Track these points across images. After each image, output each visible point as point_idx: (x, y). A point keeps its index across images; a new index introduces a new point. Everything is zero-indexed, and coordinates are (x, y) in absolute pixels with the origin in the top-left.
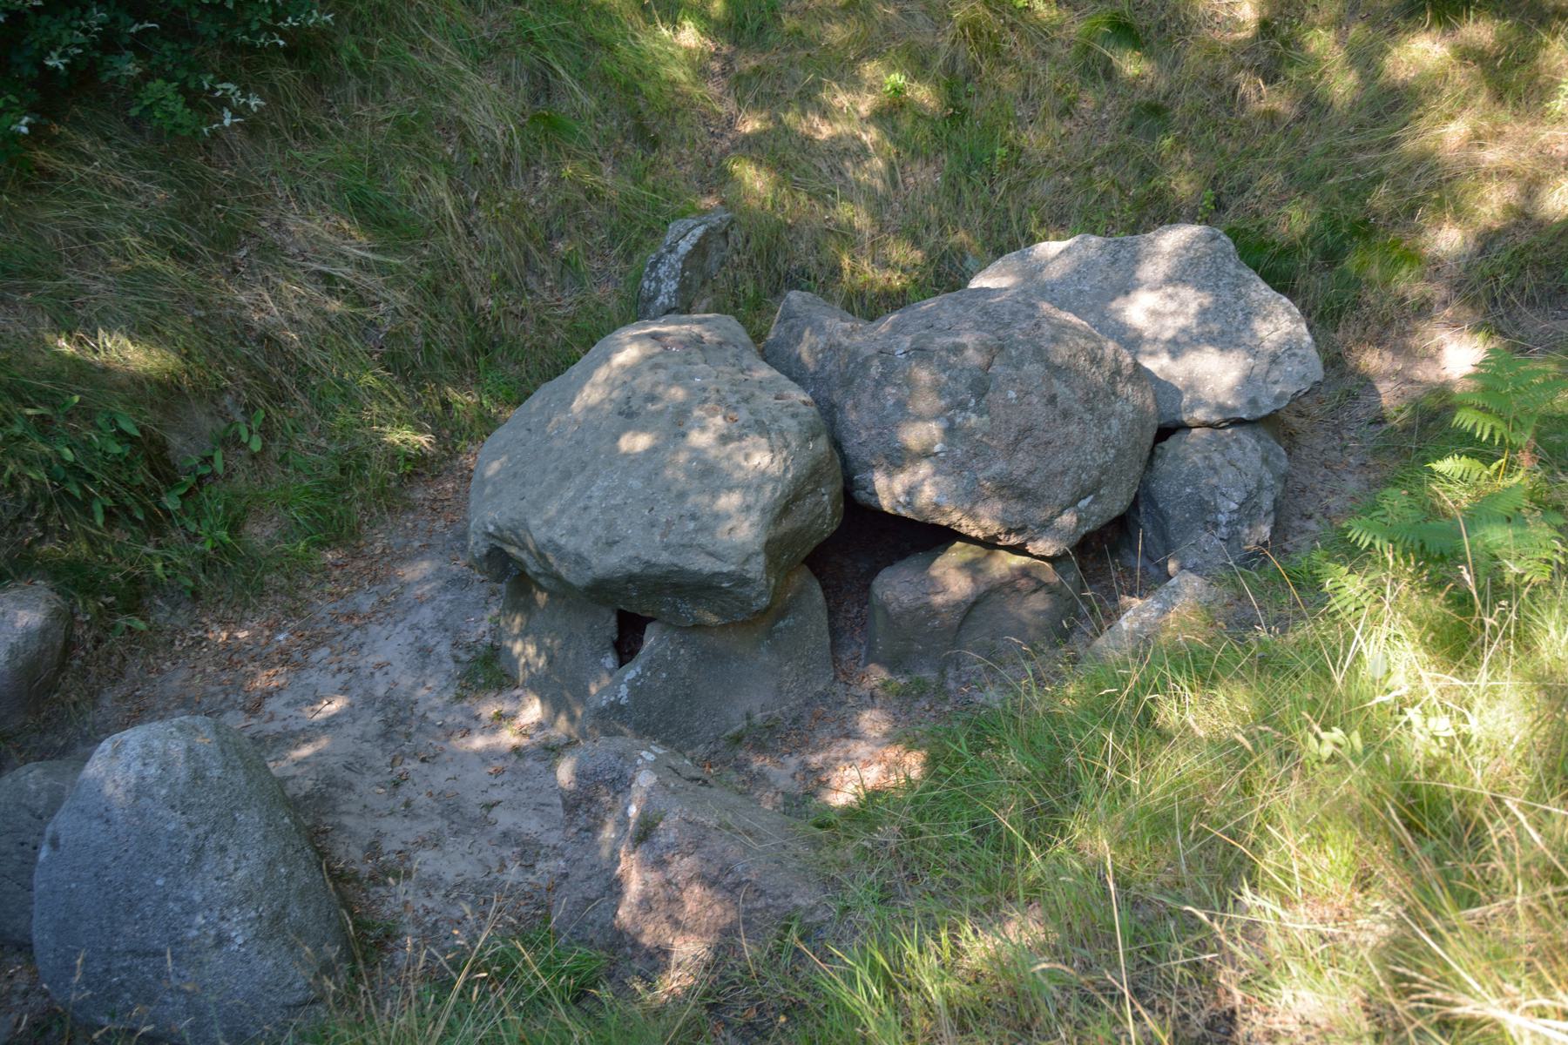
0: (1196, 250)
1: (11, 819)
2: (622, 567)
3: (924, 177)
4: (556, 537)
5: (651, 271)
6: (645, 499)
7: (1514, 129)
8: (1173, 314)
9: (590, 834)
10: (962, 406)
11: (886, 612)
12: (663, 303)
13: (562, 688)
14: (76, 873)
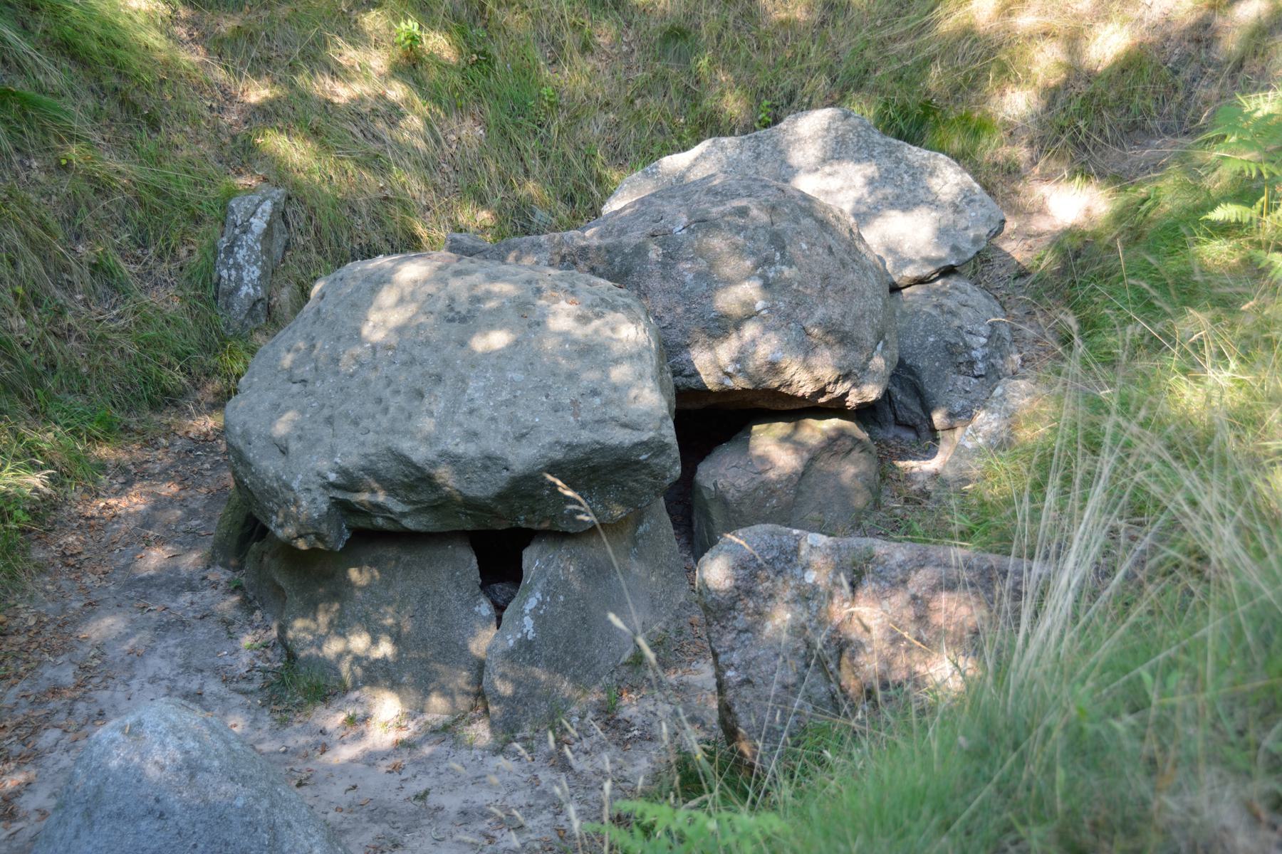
0: (837, 129)
2: (543, 457)
3: (470, 132)
4: (451, 448)
5: (227, 257)
6: (535, 387)
9: (750, 635)
10: (768, 261)
11: (725, 503)
12: (247, 294)
13: (426, 661)
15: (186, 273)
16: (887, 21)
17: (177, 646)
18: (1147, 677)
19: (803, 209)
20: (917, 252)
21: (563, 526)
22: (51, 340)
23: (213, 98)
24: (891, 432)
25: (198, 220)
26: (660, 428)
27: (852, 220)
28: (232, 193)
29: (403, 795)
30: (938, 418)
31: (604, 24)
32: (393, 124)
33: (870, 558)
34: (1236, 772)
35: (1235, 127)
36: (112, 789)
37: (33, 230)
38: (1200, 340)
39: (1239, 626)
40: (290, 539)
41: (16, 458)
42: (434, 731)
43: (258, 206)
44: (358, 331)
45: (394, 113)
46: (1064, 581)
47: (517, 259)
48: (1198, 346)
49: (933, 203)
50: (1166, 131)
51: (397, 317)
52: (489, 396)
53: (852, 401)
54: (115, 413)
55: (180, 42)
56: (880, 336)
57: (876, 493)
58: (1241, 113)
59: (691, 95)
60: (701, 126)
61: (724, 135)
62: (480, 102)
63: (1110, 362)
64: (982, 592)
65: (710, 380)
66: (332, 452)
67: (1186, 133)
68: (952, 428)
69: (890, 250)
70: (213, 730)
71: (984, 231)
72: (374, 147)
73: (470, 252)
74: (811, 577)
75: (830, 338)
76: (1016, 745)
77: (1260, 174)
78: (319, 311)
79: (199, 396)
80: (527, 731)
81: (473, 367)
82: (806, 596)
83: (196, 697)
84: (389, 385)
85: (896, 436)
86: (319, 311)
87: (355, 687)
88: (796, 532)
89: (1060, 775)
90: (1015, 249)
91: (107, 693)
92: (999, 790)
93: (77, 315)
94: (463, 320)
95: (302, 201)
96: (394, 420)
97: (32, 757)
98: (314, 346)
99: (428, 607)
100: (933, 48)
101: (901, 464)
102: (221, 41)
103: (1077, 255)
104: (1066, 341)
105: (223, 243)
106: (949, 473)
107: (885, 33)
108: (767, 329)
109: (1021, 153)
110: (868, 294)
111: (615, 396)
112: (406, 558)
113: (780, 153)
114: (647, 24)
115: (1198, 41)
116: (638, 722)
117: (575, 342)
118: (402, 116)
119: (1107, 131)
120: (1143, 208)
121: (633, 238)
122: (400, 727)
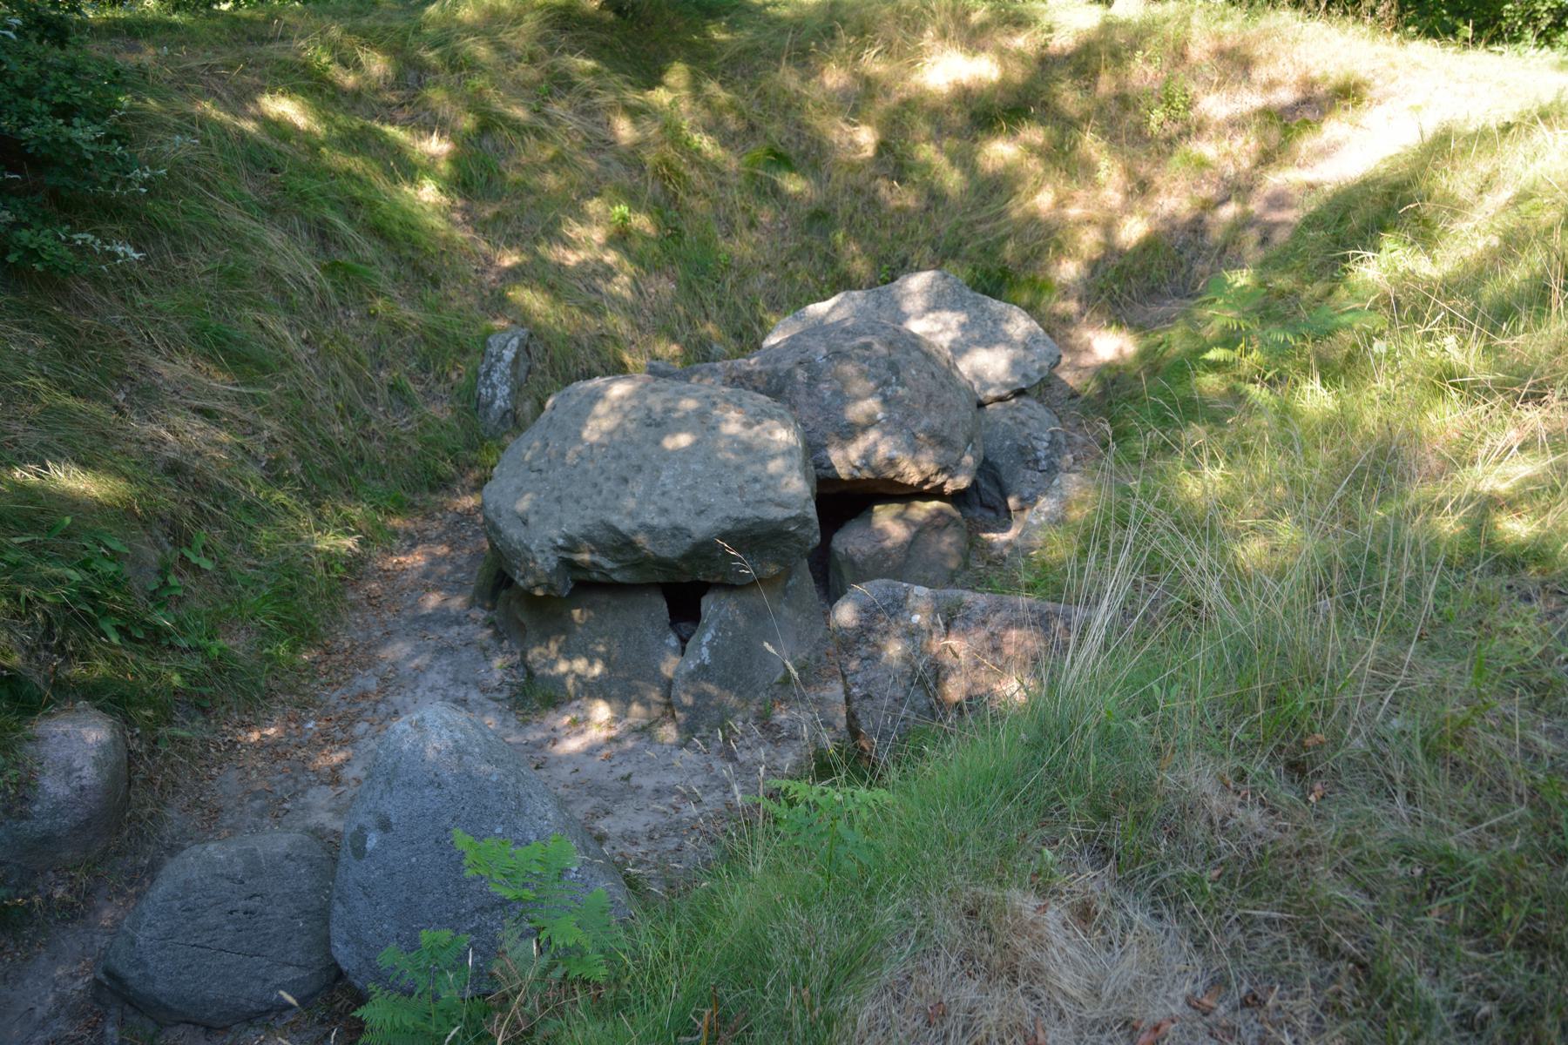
1: (212, 892)
3: (664, 287)
4: (648, 521)
7: (1081, 194)
8: (941, 331)
10: (886, 383)
11: (853, 563)
14: (415, 846)
15: (456, 391)
16: (974, 209)
17: (448, 665)
18: (1156, 689)
19: (913, 345)
20: (998, 378)
21: (731, 580)
22: (360, 441)
23: (478, 264)
24: (977, 512)
25: (464, 351)
26: (804, 507)
27: (949, 353)
28: (490, 332)
29: (613, 776)
30: (1012, 502)
31: (766, 208)
32: (609, 281)
33: (960, 605)
34: (1213, 755)
35: (1222, 293)
36: (405, 766)
37: (350, 361)
38: (1199, 446)
39: (1221, 652)
40: (530, 587)
41: (336, 526)
42: (635, 731)
43: (508, 341)
44: (579, 433)
45: (609, 273)
46: (1099, 620)
47: (700, 380)
48: (1198, 450)
49: (1008, 342)
50: (1175, 294)
51: (607, 424)
52: (677, 482)
53: (949, 488)
54: (404, 494)
55: (456, 224)
56: (970, 440)
57: (966, 556)
58: (1226, 283)
59: (830, 260)
60: (838, 283)
61: (854, 289)
62: (673, 264)
63: (1136, 461)
64: (1041, 630)
65: (843, 472)
66: (561, 523)
67: (1189, 296)
68: (1022, 509)
69: (977, 376)
70: (475, 726)
71: (1046, 364)
72: (594, 298)
73: (665, 375)
74: (916, 618)
75: (932, 441)
76: (1062, 739)
77: (1239, 328)
78: (551, 418)
79: (464, 482)
80: (704, 732)
81: (665, 460)
82: (912, 633)
83: (463, 702)
84: (602, 473)
85: (982, 515)
86: (551, 418)
87: (577, 698)
88: (905, 585)
89: (1093, 759)
90: (1068, 377)
91: (399, 698)
92: (1049, 772)
93: (379, 422)
94: (658, 425)
95: (540, 338)
96: (606, 499)
97: (352, 741)
98: (547, 445)
99: (631, 639)
100: (1008, 229)
101: (985, 536)
102: (486, 222)
103: (1114, 382)
104: (1105, 445)
105: (483, 369)
106: (1019, 543)
107: (974, 217)
108: (885, 434)
109: (1072, 306)
110: (961, 408)
111: (772, 483)
112: (614, 603)
113: (896, 304)
114: (798, 208)
115: (1195, 231)
116: (786, 725)
117: (741, 442)
118: (615, 275)
119: (1134, 293)
120: (1160, 349)
121: (786, 365)
122: (610, 728)
